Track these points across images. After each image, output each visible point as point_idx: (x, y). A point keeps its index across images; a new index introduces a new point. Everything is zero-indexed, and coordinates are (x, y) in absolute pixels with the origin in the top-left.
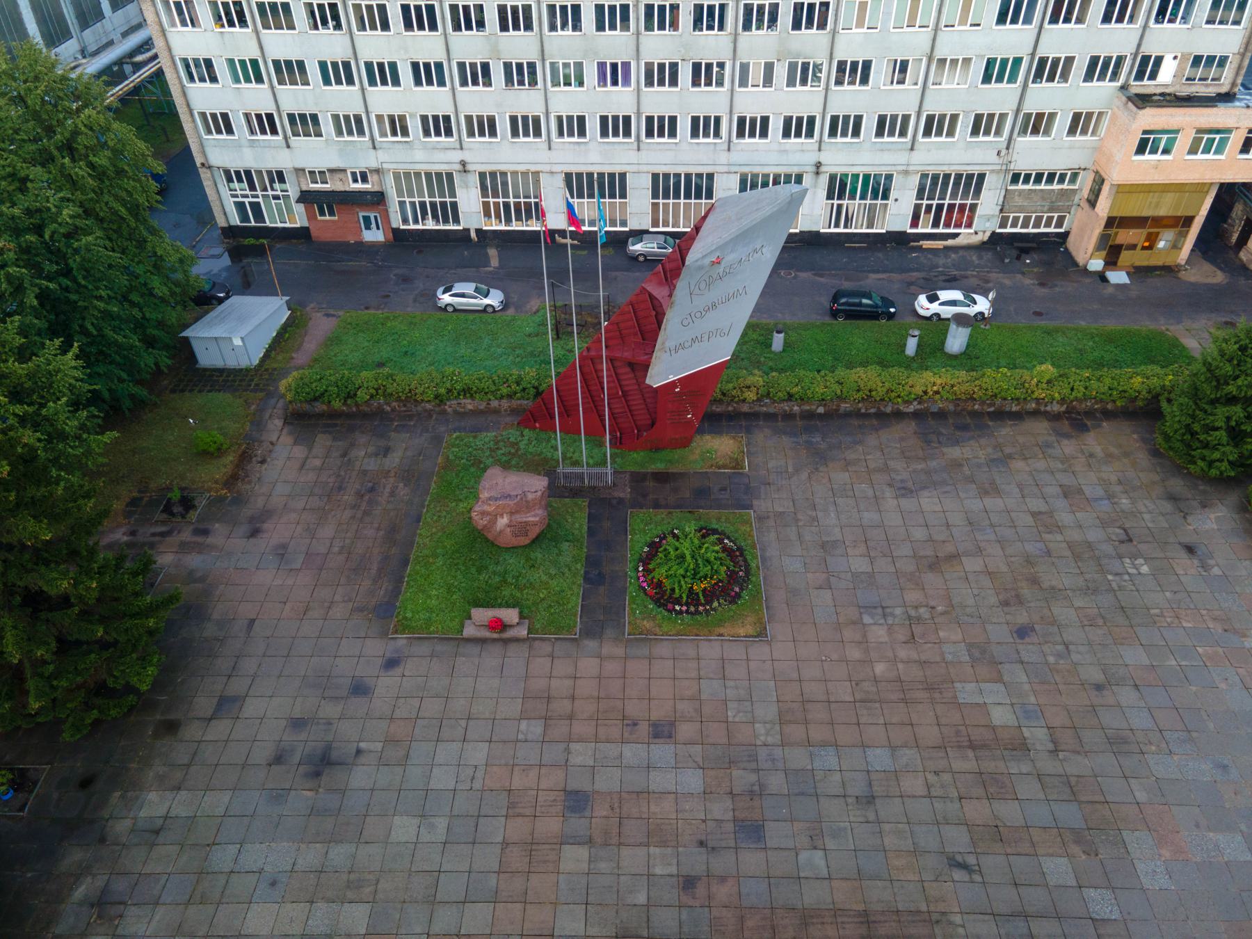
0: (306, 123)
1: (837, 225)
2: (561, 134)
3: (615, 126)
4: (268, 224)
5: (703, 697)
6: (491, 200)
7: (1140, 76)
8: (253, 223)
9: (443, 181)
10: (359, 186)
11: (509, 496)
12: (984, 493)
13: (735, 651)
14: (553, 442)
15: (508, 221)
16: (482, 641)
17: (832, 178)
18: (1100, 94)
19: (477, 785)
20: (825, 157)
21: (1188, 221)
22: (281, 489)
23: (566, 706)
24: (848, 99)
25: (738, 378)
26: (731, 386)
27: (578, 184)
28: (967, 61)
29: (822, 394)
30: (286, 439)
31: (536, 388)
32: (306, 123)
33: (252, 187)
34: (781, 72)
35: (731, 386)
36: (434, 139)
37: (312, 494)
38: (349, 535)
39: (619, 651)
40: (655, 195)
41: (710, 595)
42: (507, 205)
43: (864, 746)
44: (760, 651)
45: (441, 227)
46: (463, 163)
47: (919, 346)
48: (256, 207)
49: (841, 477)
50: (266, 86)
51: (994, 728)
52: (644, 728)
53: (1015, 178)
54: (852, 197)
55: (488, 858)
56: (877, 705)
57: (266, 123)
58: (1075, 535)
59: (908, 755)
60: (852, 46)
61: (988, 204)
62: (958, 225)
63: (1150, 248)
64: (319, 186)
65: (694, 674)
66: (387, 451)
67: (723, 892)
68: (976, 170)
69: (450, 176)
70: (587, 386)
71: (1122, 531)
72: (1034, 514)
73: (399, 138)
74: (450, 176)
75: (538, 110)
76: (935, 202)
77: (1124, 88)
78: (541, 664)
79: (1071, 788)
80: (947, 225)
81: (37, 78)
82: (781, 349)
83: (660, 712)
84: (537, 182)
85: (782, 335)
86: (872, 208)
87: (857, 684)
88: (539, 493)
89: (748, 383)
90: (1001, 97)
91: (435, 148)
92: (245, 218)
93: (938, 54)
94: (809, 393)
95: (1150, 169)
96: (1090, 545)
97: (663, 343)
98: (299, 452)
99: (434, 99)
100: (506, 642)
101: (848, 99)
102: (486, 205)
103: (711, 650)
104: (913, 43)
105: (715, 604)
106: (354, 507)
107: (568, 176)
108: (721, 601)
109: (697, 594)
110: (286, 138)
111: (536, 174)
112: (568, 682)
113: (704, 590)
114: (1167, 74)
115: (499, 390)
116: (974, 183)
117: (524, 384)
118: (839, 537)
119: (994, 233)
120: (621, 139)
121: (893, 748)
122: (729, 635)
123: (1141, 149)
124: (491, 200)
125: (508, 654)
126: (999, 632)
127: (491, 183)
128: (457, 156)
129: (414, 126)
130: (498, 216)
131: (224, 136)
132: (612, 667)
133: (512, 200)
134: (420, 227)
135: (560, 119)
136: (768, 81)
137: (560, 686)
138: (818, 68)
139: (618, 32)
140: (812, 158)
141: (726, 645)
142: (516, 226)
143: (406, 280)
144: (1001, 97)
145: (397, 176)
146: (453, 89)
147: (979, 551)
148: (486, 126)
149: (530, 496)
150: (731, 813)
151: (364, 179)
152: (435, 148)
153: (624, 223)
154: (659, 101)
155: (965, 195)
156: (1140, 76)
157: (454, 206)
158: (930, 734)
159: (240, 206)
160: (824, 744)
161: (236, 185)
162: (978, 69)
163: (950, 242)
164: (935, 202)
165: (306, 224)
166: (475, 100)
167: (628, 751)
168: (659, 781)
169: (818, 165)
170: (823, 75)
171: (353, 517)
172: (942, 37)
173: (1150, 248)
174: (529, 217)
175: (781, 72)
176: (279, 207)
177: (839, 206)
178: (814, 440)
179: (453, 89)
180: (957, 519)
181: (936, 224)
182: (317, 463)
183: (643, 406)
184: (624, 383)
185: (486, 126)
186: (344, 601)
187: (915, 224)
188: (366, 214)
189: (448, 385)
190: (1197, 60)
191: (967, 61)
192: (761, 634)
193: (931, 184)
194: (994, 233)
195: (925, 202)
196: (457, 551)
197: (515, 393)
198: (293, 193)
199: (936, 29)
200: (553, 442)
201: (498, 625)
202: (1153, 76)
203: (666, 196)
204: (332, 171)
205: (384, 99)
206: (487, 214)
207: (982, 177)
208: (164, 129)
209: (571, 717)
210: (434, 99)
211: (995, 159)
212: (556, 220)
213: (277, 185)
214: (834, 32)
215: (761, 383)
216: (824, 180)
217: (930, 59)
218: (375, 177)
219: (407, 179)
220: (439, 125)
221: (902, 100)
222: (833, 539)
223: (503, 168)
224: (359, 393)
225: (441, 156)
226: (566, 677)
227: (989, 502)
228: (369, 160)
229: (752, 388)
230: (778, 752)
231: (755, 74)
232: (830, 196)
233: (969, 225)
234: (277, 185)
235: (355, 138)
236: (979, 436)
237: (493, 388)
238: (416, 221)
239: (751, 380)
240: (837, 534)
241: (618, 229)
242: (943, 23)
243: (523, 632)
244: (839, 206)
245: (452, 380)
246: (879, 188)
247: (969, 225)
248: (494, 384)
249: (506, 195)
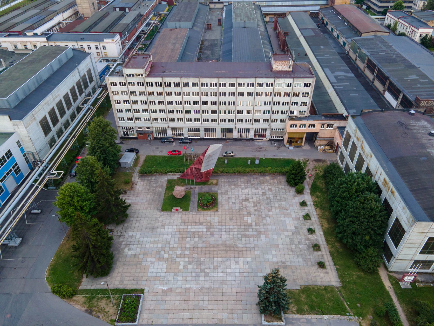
0: (139, 119)
1: (240, 137)
2: (187, 121)
3: (197, 120)
4: (129, 136)
6: (174, 132)
7: (291, 113)
8: (126, 136)
9: (164, 129)
10: (148, 130)
12: (256, 189)
13: (213, 213)
15: (177, 136)
16: (175, 212)
17: (238, 129)
18: (284, 116)
19: (175, 231)
20: (237, 126)
21: (302, 139)
22: (140, 189)
23: (187, 221)
24: (240, 116)
27: (190, 130)
28: (260, 111)
30: (140, 180)
32: (139, 119)
33: (127, 130)
34: (227, 112)
36: (163, 122)
37: (145, 190)
39: (195, 214)
40: (205, 132)
41: (210, 205)
42: (177, 133)
43: (229, 225)
44: (216, 213)
45: (164, 137)
46: (168, 126)
47: (251, 162)
48: (127, 133)
49: (233, 187)
50: (132, 113)
51: (248, 223)
52: (198, 224)
53: (272, 129)
54: (242, 132)
55: (177, 239)
57: (131, 119)
58: (268, 196)
59: (235, 227)
60: (239, 108)
61: (268, 134)
62: (263, 137)
63: (297, 143)
64: (140, 130)
66: (157, 182)
67: (208, 243)
68: (265, 128)
69: (166, 128)
72: (263, 193)
73: (156, 122)
74: (166, 128)
75: (183, 117)
76: (258, 133)
77: (288, 115)
78: (184, 216)
79: (256, 230)
80: (261, 137)
81: (102, 123)
83: (201, 221)
84: (182, 130)
86: (246, 134)
90: (267, 116)
91: (163, 123)
92: (125, 135)
93: (255, 110)
95: (293, 130)
96: (270, 197)
98: (142, 183)
99: (163, 115)
100: (178, 212)
101: (240, 116)
102: (173, 133)
103: (209, 213)
104: (250, 108)
107: (188, 128)
110: (134, 122)
111: (182, 128)
114: (295, 113)
116: (265, 130)
119: (270, 139)
120: (198, 122)
121: (233, 225)
123: (291, 127)
124: (174, 132)
126: (252, 210)
127: (174, 129)
128: (167, 125)
129: (159, 120)
130: (175, 135)
131: (123, 121)
132: (194, 216)
133: (178, 132)
134: (160, 137)
135: (187, 119)
136: (225, 113)
137: (187, 218)
138: (234, 111)
139: (197, 105)
140: (234, 126)
142: (178, 137)
143: (157, 148)
144: (267, 116)
145: (155, 128)
146: (167, 114)
147: (252, 198)
148: (173, 120)
151: (149, 128)
152: (163, 123)
153: (199, 136)
154: (205, 116)
155: (263, 132)
156: (291, 113)
157: (166, 133)
158: (239, 224)
159: (124, 133)
160: (224, 225)
161: (124, 129)
162: (262, 112)
163: (262, 140)
164: (258, 133)
165: (137, 136)
166: (171, 116)
167: (196, 227)
168: (200, 230)
169: (235, 127)
170: (235, 112)
172: (255, 106)
173: (297, 143)
174: (181, 135)
175: (227, 112)
176: (132, 133)
177: (240, 134)
179: (167, 114)
180: (250, 193)
181: (259, 137)
182: (146, 185)
185: (173, 120)
187: (255, 137)
188: (81, 44)
190: (300, 111)
191: (260, 111)
192: (217, 211)
193: (256, 130)
194: (270, 139)
195: (256, 133)
198: (135, 131)
199: (254, 106)
202: (293, 114)
203: (207, 132)
204: (143, 127)
205: (154, 115)
206: (173, 134)
207: (266, 129)
208: (103, 112)
209: (188, 222)
210: (163, 115)
211: (268, 126)
212: (187, 136)
213: (132, 129)
214: (236, 106)
216: (237, 130)
217: (253, 110)
218: (151, 128)
219: (157, 129)
220: (164, 120)
221: (250, 116)
223: (176, 127)
225: (163, 125)
227: (256, 191)
228: (150, 125)
230: (217, 226)
231: (222, 112)
232: (238, 132)
233: (265, 137)
234: (132, 129)
235: (148, 122)
236: (328, 168)
238: (159, 136)
239: (220, 169)
240: (231, 196)
241: (198, 137)
242: (255, 105)
243: (181, 211)
244: (240, 134)
246: (247, 130)
247: (265, 137)
249: (176, 131)
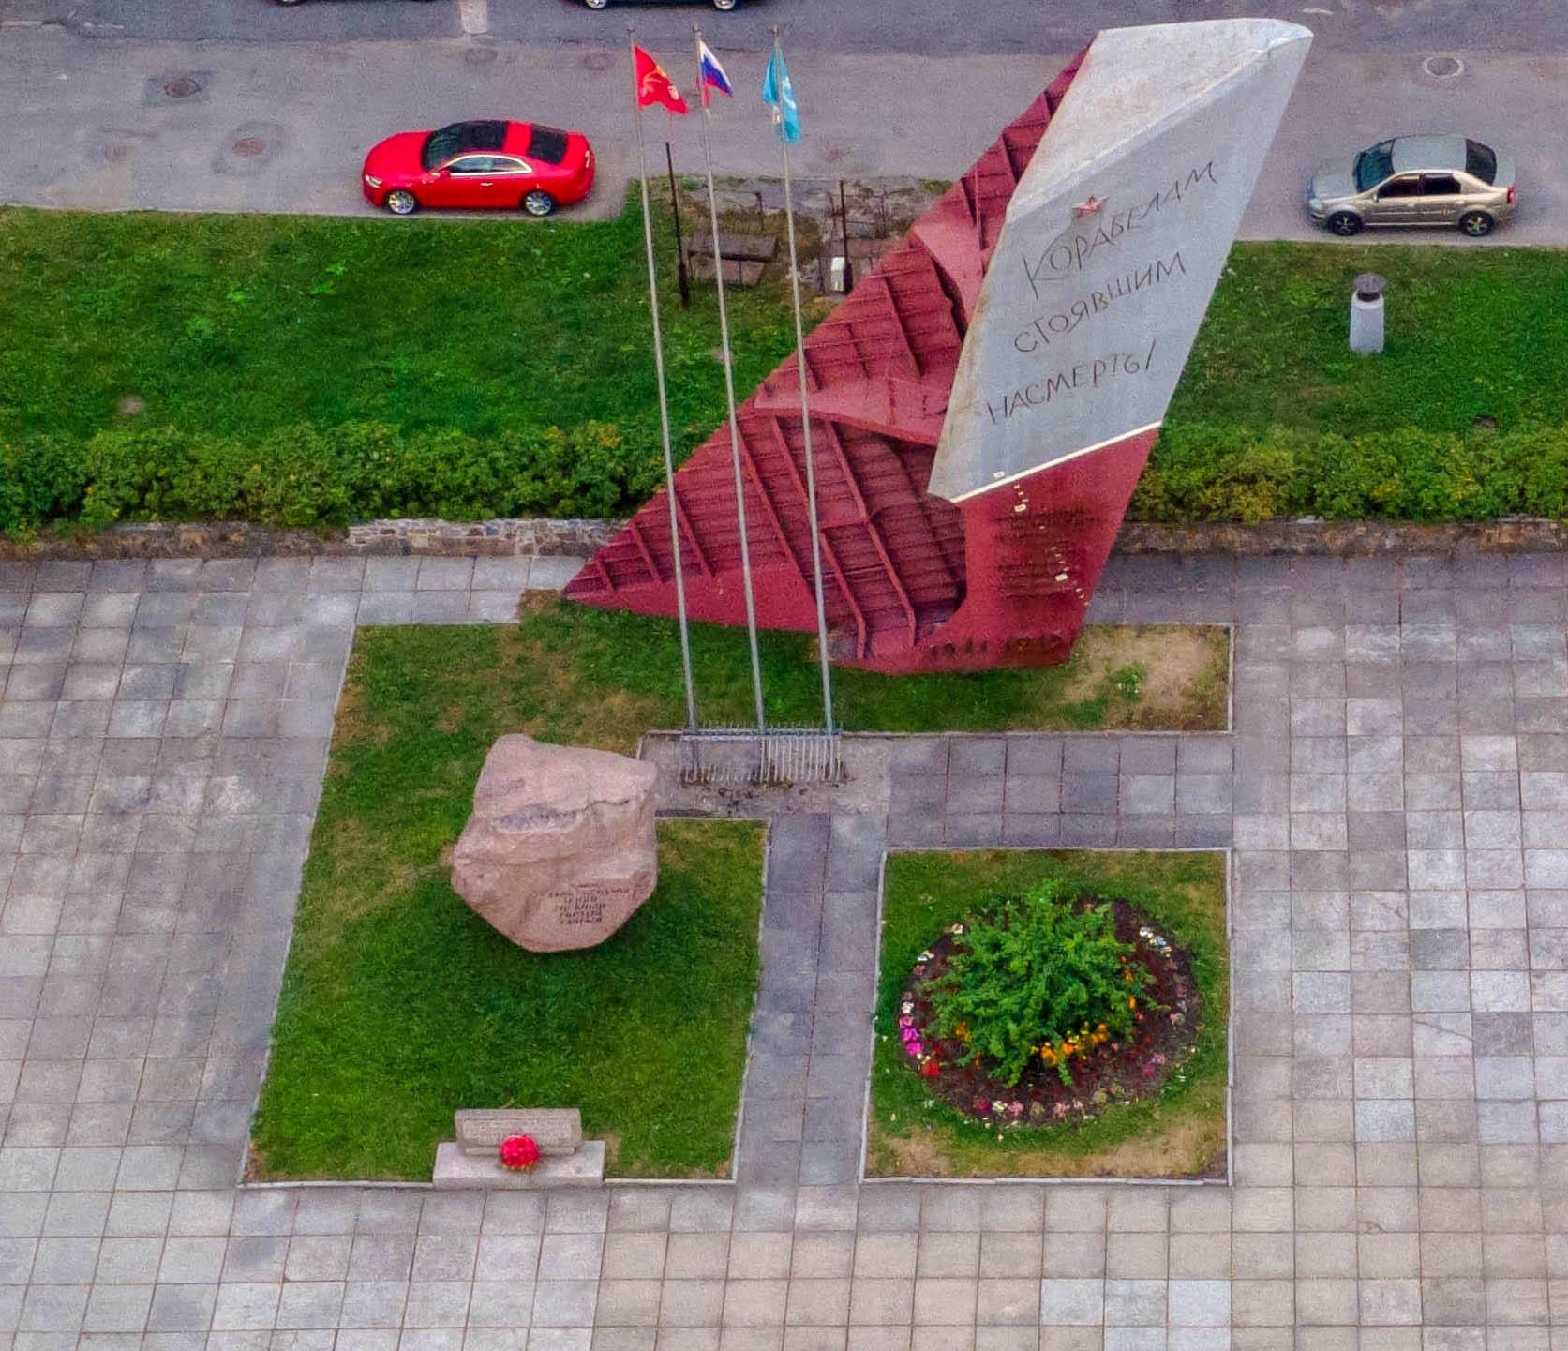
5: (1045, 1320)
11: (555, 814)
13: (1141, 1211)
14: (669, 647)
16: (479, 1192)
25: (1220, 453)
26: (1195, 476)
29: (1464, 503)
31: (621, 482)
35: (1195, 476)
38: (98, 924)
39: (842, 1216)
41: (1085, 1069)
44: (1201, 1207)
56: (1476, 1332)
65: (1028, 1267)
70: (693, 525)
71: (58, 27)
82: (1378, 343)
85: (1378, 304)
87: (1437, 1286)
88: (633, 806)
89: (1246, 467)
94: (1426, 496)
97: (969, 394)
100: (548, 1193)
105: (1100, 1096)
106: (106, 846)
108: (1115, 1089)
109: (1055, 1071)
112: (710, 1292)
113: (1072, 1060)
115: (510, 487)
117: (583, 474)
118: (1457, 920)
122: (1128, 1174)
125: (552, 1227)
141: (1118, 1197)
143: (182, 88)
149: (609, 815)
150: (1053, 1217)
171: (103, 876)
178: (1434, 640)
183: (939, 565)
184: (875, 484)
186: (107, 1102)
189: (356, 475)
196: (410, 963)
197: (555, 499)
200: (669, 647)
201: (521, 1154)
215: (1289, 467)
222: (1439, 924)
224: (88, 501)
226: (705, 1279)
229: (1262, 482)
237: (492, 484)
239: (1258, 456)
245: (368, 458)
248: (496, 473)
